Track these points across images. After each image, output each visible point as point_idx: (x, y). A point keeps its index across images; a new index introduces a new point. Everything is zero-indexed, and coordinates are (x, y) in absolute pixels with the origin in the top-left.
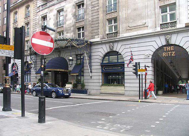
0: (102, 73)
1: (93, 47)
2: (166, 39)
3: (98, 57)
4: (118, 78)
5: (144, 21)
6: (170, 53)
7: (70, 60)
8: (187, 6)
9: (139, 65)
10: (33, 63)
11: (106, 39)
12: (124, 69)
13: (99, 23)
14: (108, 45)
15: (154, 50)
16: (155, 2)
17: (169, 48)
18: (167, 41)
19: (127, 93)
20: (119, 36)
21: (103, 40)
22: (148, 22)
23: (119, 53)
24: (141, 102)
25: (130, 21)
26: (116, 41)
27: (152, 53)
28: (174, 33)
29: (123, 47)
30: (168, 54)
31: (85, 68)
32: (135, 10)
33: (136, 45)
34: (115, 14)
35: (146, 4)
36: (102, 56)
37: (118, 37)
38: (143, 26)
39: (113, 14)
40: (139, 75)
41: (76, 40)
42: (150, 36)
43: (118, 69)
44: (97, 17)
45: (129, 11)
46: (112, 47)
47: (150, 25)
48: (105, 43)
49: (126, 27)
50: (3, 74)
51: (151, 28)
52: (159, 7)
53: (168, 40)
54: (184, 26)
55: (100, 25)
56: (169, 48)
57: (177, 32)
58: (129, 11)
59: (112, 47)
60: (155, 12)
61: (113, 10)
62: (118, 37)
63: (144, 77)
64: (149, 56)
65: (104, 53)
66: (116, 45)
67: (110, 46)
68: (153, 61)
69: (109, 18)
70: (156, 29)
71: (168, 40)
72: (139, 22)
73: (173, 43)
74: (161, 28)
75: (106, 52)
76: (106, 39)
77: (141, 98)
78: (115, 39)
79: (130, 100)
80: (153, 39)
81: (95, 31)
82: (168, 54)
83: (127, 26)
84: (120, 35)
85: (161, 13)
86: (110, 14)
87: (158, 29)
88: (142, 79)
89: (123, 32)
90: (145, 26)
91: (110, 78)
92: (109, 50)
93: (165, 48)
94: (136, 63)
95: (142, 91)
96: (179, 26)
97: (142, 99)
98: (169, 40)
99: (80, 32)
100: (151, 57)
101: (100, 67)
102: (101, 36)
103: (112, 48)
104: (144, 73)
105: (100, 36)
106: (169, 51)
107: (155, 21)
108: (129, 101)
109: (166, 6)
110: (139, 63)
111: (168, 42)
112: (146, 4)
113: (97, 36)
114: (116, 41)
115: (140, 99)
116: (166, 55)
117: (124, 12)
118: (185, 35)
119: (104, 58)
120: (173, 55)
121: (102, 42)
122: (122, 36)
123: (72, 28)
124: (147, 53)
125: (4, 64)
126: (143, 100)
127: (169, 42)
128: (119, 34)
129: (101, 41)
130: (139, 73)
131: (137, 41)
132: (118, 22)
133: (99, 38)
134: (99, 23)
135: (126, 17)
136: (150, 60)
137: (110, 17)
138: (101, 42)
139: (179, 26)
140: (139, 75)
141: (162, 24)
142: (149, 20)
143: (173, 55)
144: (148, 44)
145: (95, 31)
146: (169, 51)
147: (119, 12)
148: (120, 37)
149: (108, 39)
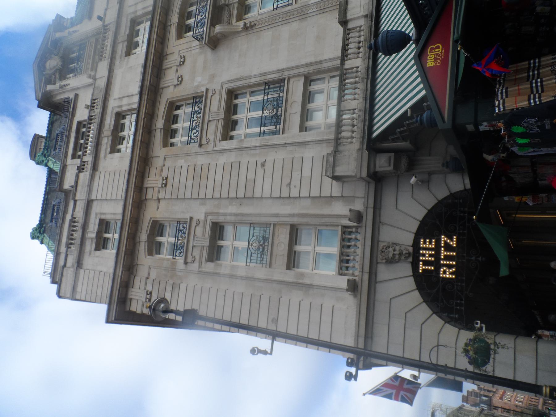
30: (447, 258)
73: (407, 239)
82: (447, 258)
93: (422, 267)
106: (438, 253)
116: (450, 267)
120: (454, 244)
143: (454, 244)
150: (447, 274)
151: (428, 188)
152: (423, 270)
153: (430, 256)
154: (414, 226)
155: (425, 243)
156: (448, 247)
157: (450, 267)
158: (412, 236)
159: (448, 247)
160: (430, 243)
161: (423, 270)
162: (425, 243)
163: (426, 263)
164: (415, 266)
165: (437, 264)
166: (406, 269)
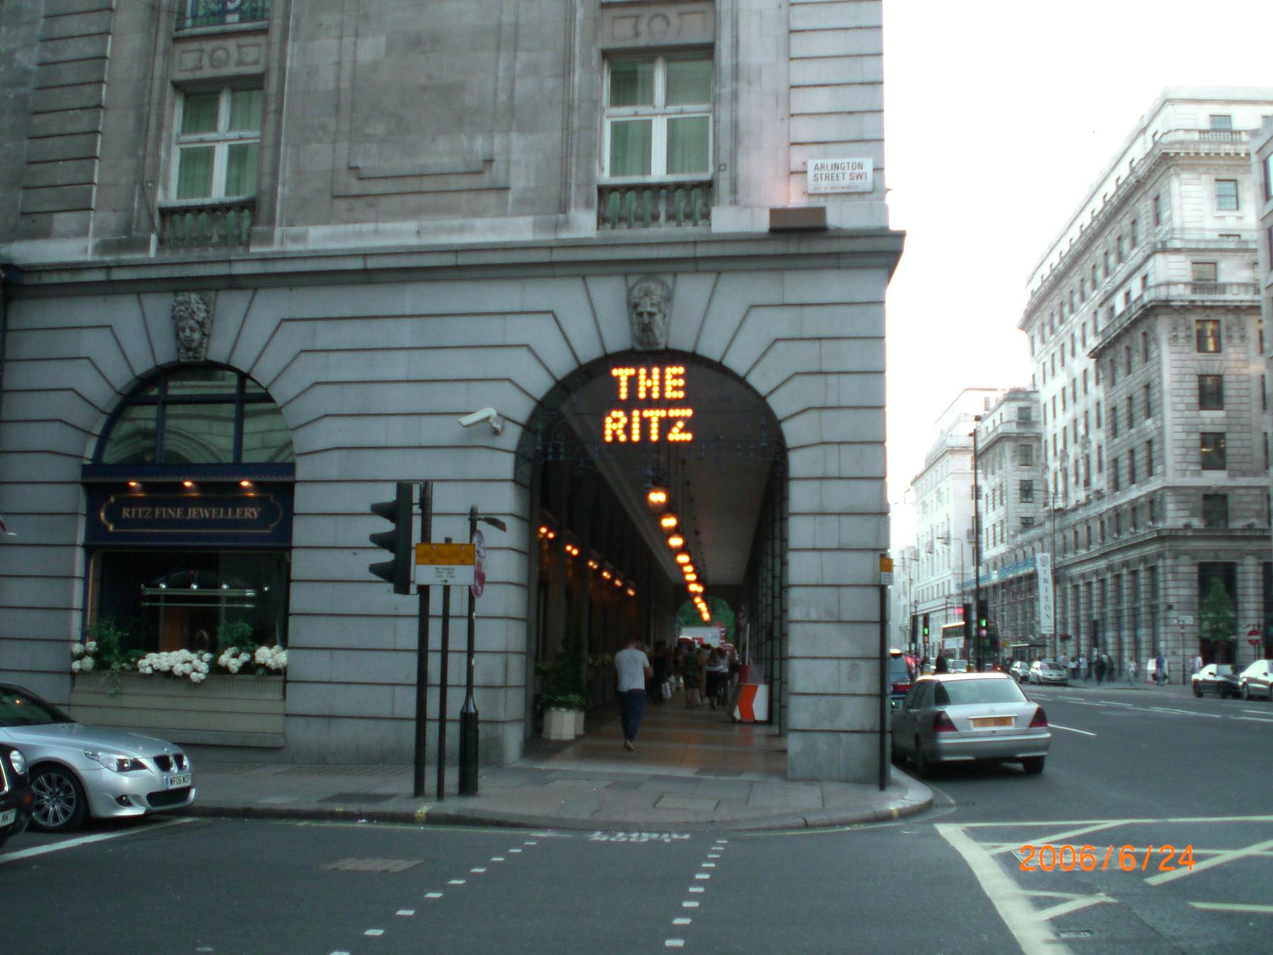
0: (89, 549)
1: (29, 314)
2: (633, 307)
3: (62, 406)
4: (231, 600)
5: (480, 145)
6: (655, 415)
8: (783, 87)
9: (425, 502)
10: (1028, 622)
11: (152, 253)
12: (286, 531)
13: (99, 106)
14: (159, 307)
15: (540, 385)
16: (570, 12)
17: (649, 376)
18: (642, 322)
19: (305, 735)
20: (268, 239)
21: (128, 257)
22: (508, 161)
23: (249, 383)
24: (431, 819)
25: (369, 130)
26: (234, 283)
27: (522, 409)
28: (694, 264)
29: (295, 337)
30: (645, 423)
32: (416, 43)
33: (404, 333)
34: (252, 54)
35: (507, 18)
36: (104, 396)
37: (255, 249)
38: (466, 182)
39: (231, 44)
40: (424, 591)
43: (161, 523)
44: (89, 49)
45: (370, 48)
46: (201, 324)
47: (519, 183)
48: (137, 288)
49: (333, 171)
50: (217, 670)
51: (526, 205)
52: (596, 54)
53: (646, 318)
54: (762, 224)
55: (106, 121)
56: (649, 376)
57: (712, 265)
58: (370, 48)
59: (201, 324)
60: (567, 87)
61: (235, 17)
62: (255, 249)
63: (458, 605)
64: (496, 432)
65: (121, 378)
66: (231, 306)
67: (176, 319)
68: (526, 469)
69: (199, 75)
70: (561, 217)
71: (651, 314)
72: (442, 144)
73: (681, 339)
74: (602, 220)
75: (143, 365)
76: (152, 253)
77: (431, 781)
78: (230, 262)
79: (339, 808)
80: (538, 294)
81: (63, 173)
82: (645, 423)
83: (342, 164)
84: (278, 232)
85: (606, 97)
86: (208, 46)
87: (584, 223)
88: (446, 617)
89: (305, 212)
90: (484, 181)
91: (155, 598)
92: (166, 354)
93: (623, 374)
94: (404, 488)
95: (442, 720)
96: (725, 220)
97: (440, 794)
98: (658, 318)
100: (511, 437)
101: (76, 499)
102: (103, 219)
103: (197, 336)
104: (463, 575)
105: (93, 220)
106: (650, 403)
107: (565, 159)
108: (333, 816)
109: (650, 54)
110: (426, 487)
111: (647, 329)
112: (507, 18)
113: (63, 221)
114: (234, 283)
115: (419, 791)
116: (628, 429)
117: (327, 43)
118: (761, 287)
119: (114, 418)
120: (676, 435)
121: (118, 275)
122: (292, 247)
126: (452, 806)
127: (657, 332)
128: (271, 222)
129: (108, 268)
130: (422, 574)
131: (411, 298)
133: (90, 242)
134: (99, 106)
135: (338, 90)
136: (505, 465)
137: (208, 72)
138: (100, 276)
139: (725, 220)
140: (424, 591)
141: (614, 189)
142: (517, 140)
144: (493, 330)
145: (63, 173)
147: (284, 38)
148: (275, 248)
149: (168, 256)
150: (614, 425)
151: (752, 306)
152: (618, 378)
153: (649, 390)
154: (711, 349)
155: (676, 377)
156: (666, 424)
157: (628, 429)
159: (666, 424)
160: (676, 388)
161: (618, 378)
162: (676, 377)
163: (633, 382)
165: (633, 403)
166: (619, 338)
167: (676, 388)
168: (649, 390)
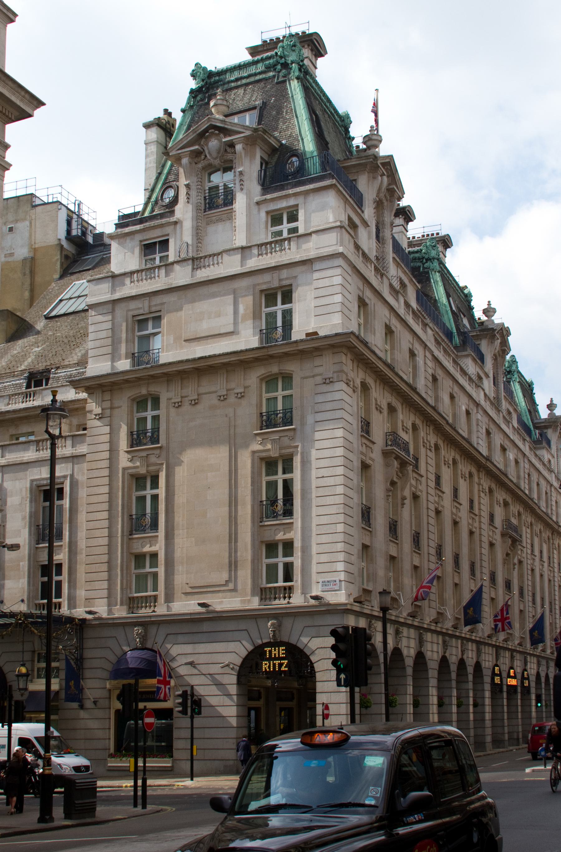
6: (277, 662)
7: (20, 675)
17: (275, 650)
30: (274, 665)
31: (77, 350)
41: (194, 114)
42: (186, 628)
56: (275, 650)
82: (274, 665)
93: (268, 649)
99: (146, 413)
106: (275, 659)
116: (269, 667)
120: (283, 668)
123: (21, 563)
124: (227, 659)
125: (366, 684)
132: (124, 599)
143: (283, 668)
146: (275, 659)
150: (265, 666)
153: (275, 654)
154: (293, 641)
155: (283, 650)
156: (281, 665)
157: (269, 667)
158: (285, 639)
159: (281, 665)
160: (283, 654)
162: (283, 650)
164: (268, 644)
165: (270, 659)
167: (283, 654)
168: (275, 654)
